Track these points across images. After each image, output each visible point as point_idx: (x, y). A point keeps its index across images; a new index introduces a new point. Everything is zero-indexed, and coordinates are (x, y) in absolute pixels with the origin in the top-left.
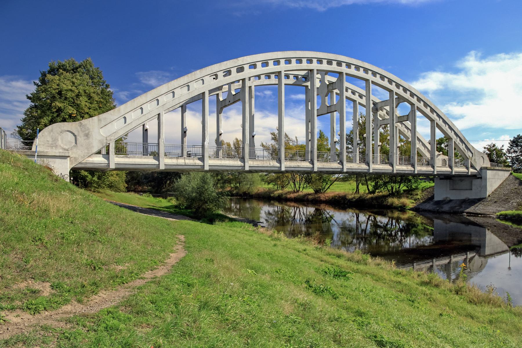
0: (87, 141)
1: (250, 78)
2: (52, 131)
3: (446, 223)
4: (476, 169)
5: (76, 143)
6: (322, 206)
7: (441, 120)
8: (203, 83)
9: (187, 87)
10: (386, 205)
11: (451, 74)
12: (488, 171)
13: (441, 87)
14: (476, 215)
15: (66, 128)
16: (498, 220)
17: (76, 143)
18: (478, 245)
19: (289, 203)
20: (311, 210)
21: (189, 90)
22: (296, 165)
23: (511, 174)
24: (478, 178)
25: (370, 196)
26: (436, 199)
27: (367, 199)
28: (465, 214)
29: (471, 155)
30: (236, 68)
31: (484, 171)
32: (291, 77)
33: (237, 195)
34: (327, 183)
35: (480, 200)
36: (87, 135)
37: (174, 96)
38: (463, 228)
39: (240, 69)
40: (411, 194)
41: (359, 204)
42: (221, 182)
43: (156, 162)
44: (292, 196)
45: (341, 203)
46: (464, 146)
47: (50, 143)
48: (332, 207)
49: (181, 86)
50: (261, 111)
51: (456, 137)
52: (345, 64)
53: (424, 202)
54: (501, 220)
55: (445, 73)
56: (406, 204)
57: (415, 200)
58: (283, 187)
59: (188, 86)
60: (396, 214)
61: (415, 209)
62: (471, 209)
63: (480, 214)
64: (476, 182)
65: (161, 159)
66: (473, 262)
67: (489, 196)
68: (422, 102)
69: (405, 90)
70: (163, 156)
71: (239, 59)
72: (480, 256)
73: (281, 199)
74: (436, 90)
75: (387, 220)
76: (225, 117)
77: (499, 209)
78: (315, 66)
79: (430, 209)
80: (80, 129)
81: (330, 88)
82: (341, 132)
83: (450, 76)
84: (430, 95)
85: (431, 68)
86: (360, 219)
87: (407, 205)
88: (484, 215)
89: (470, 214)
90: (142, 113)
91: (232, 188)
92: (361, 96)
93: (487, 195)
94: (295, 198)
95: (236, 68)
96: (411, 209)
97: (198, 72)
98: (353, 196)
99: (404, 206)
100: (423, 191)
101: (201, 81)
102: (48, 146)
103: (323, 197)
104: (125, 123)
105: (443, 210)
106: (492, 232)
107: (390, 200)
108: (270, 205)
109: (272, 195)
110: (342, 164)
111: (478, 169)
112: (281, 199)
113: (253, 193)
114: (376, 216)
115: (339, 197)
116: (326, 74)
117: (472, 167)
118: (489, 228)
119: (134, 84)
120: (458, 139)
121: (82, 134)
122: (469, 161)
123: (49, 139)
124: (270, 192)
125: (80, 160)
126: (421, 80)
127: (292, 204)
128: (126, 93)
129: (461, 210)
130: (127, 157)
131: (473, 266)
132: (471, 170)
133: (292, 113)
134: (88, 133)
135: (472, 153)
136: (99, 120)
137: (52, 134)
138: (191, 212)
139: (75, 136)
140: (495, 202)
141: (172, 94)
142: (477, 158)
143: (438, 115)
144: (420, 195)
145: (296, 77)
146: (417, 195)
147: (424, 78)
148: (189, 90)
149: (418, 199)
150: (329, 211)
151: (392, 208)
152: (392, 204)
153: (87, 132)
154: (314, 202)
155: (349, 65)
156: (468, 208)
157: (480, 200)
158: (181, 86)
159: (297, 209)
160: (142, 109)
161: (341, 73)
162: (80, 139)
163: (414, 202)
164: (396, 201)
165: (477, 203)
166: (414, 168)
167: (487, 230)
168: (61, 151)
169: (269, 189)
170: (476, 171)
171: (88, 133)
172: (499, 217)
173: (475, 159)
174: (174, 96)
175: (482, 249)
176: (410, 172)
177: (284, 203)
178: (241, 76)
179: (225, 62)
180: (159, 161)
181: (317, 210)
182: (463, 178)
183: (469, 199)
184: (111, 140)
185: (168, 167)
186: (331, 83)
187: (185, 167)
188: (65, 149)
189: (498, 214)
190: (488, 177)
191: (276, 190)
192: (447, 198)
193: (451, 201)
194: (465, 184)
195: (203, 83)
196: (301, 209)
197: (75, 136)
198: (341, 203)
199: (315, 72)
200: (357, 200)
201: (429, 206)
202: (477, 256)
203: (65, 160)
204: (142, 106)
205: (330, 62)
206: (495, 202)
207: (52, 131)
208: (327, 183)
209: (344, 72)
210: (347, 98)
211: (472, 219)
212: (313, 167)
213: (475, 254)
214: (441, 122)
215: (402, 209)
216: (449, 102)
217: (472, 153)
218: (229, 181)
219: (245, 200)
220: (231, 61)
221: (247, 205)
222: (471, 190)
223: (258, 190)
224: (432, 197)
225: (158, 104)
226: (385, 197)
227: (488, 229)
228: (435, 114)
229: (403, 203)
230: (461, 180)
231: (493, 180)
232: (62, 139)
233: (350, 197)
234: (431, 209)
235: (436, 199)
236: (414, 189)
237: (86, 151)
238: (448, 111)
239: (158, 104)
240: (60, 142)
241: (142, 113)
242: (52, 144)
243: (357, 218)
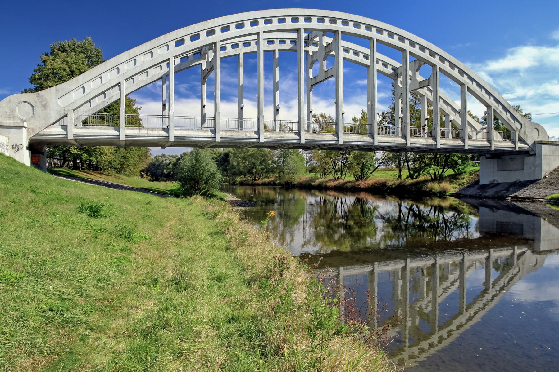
0: (44, 112)
2: (10, 102)
3: (494, 212)
4: (527, 144)
5: (34, 114)
6: (363, 195)
7: (475, 84)
8: (168, 49)
10: (425, 191)
11: (547, 47)
12: (543, 146)
13: (536, 64)
14: (523, 199)
15: (23, 100)
16: (548, 205)
17: (34, 114)
18: (532, 238)
19: (328, 192)
20: (350, 200)
21: (152, 57)
22: (278, 136)
24: (532, 155)
27: (407, 186)
28: (509, 199)
29: (519, 126)
31: (537, 146)
32: (288, 42)
33: (280, 184)
34: (369, 169)
36: (45, 106)
37: (135, 64)
38: (514, 218)
40: (457, 179)
41: (399, 192)
42: (265, 171)
43: (116, 133)
44: (332, 184)
45: (381, 191)
46: (509, 115)
47: (8, 114)
50: (326, 99)
51: (496, 105)
52: (408, 41)
53: (468, 187)
54: (552, 205)
55: (539, 47)
56: (447, 189)
57: (459, 185)
58: (325, 174)
59: (151, 52)
60: (437, 202)
61: (456, 195)
62: (519, 193)
63: (528, 198)
64: (529, 160)
66: (522, 259)
67: (545, 177)
68: (446, 62)
70: (124, 126)
71: (209, 21)
72: (533, 252)
73: (321, 188)
74: (529, 68)
75: (429, 209)
76: (288, 107)
77: (552, 192)
79: (472, 194)
80: (37, 100)
81: (327, 50)
83: (545, 50)
84: (521, 74)
85: (520, 42)
87: (448, 191)
88: (533, 200)
89: (516, 199)
90: (102, 82)
91: (276, 177)
92: (366, 57)
93: (543, 176)
94: (335, 186)
95: (206, 31)
96: (452, 195)
97: (162, 37)
98: (393, 183)
99: (445, 192)
101: (166, 47)
102: (6, 117)
103: (363, 184)
104: (84, 92)
105: (487, 194)
106: (550, 222)
107: (430, 185)
108: (312, 195)
109: (313, 184)
110: (338, 136)
111: (530, 143)
112: (321, 188)
113: (296, 183)
114: (419, 205)
115: (380, 184)
116: (323, 35)
117: (521, 140)
118: (544, 217)
119: (193, 76)
120: (500, 107)
121: (39, 105)
123: (7, 110)
124: (312, 180)
125: (37, 131)
126: (509, 57)
127: (332, 193)
128: (185, 85)
129: (507, 194)
130: (86, 128)
131: (523, 264)
132: (519, 145)
133: (360, 101)
134: (46, 104)
135: (521, 124)
136: (57, 90)
137: (9, 105)
139: (33, 107)
140: (551, 184)
141: (133, 61)
142: (528, 130)
143: (470, 78)
144: (466, 179)
146: (463, 179)
147: (512, 53)
148: (152, 57)
150: (372, 202)
151: (431, 194)
152: (431, 190)
153: (44, 103)
154: (354, 190)
155: (412, 44)
156: (515, 192)
158: (144, 53)
159: (338, 199)
161: (336, 32)
162: (38, 110)
163: (457, 186)
164: (436, 187)
165: (528, 185)
166: (436, 141)
167: (542, 220)
168: (19, 121)
169: (311, 178)
170: (528, 147)
171: (46, 104)
172: (549, 202)
173: (525, 132)
174: (135, 64)
175: (536, 244)
176: (431, 146)
177: (324, 191)
180: (119, 132)
181: (358, 201)
182: (513, 156)
183: (520, 182)
184: (68, 110)
185: (130, 138)
186: (329, 45)
187: (148, 138)
188: (22, 120)
189: (549, 197)
190: (543, 153)
191: (318, 179)
192: (494, 181)
195: (168, 49)
196: (343, 200)
197: (33, 107)
198: (381, 191)
200: (396, 187)
201: (473, 191)
202: (529, 253)
203: (20, 130)
205: (321, 20)
207: (10, 102)
208: (369, 169)
210: (378, 71)
211: (519, 204)
212: (300, 139)
213: (526, 249)
214: (474, 86)
215: (442, 195)
216: (548, 80)
217: (521, 124)
218: (272, 170)
219: (287, 189)
221: (291, 196)
222: (523, 170)
223: (301, 179)
224: (478, 181)
225: (118, 73)
226: (426, 181)
227: (545, 219)
228: (466, 76)
229: (443, 188)
230: (512, 159)
231: (552, 158)
232: (20, 110)
233: (390, 183)
234: (478, 196)
235: (482, 182)
236: (462, 173)
237: (44, 122)
238: (546, 90)
239: (118, 73)
240: (17, 113)
241: (102, 82)
242: (10, 115)
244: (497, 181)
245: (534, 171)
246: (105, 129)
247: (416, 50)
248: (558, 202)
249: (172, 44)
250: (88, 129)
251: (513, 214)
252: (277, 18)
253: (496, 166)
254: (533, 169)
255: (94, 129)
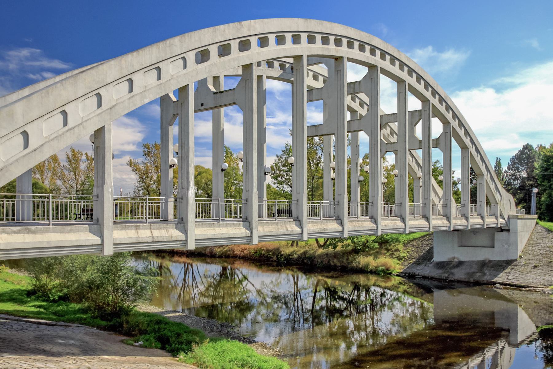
1: (259, 64)
8: (185, 67)
9: (155, 72)
12: (519, 221)
21: (159, 78)
23: (537, 223)
25: (321, 251)
26: (437, 258)
30: (238, 40)
31: (511, 220)
35: (509, 263)
37: (131, 90)
39: (244, 45)
43: (95, 239)
48: (256, 266)
49: (145, 69)
64: (499, 236)
65: (106, 233)
69: (441, 100)
70: (111, 224)
72: (509, 344)
78: (256, 53)
82: (246, 154)
86: (300, 284)
90: (65, 123)
95: (238, 40)
97: (176, 40)
100: (405, 245)
101: (181, 62)
104: (26, 145)
115: (268, 251)
122: (499, 206)
130: (29, 231)
135: (501, 196)
138: (84, 311)
140: (535, 267)
141: (127, 83)
145: (282, 66)
148: (159, 78)
149: (404, 257)
157: (509, 263)
158: (145, 69)
160: (64, 113)
174: (131, 90)
175: (511, 334)
178: (246, 57)
179: (222, 27)
180: (102, 236)
192: (454, 258)
193: (461, 263)
194: (483, 240)
199: (345, 60)
202: (507, 348)
204: (66, 108)
206: (535, 267)
209: (379, 66)
212: (343, 231)
220: (231, 25)
225: (100, 105)
235: (437, 258)
239: (100, 105)
241: (65, 123)
243: (296, 284)
244: (458, 258)
245: (508, 249)
246: (71, 231)
247: (273, 50)
248: (552, 290)
249: (191, 57)
250: (34, 232)
251: (505, 303)
252: (307, 34)
253: (456, 240)
254: (506, 247)
255: (47, 232)
